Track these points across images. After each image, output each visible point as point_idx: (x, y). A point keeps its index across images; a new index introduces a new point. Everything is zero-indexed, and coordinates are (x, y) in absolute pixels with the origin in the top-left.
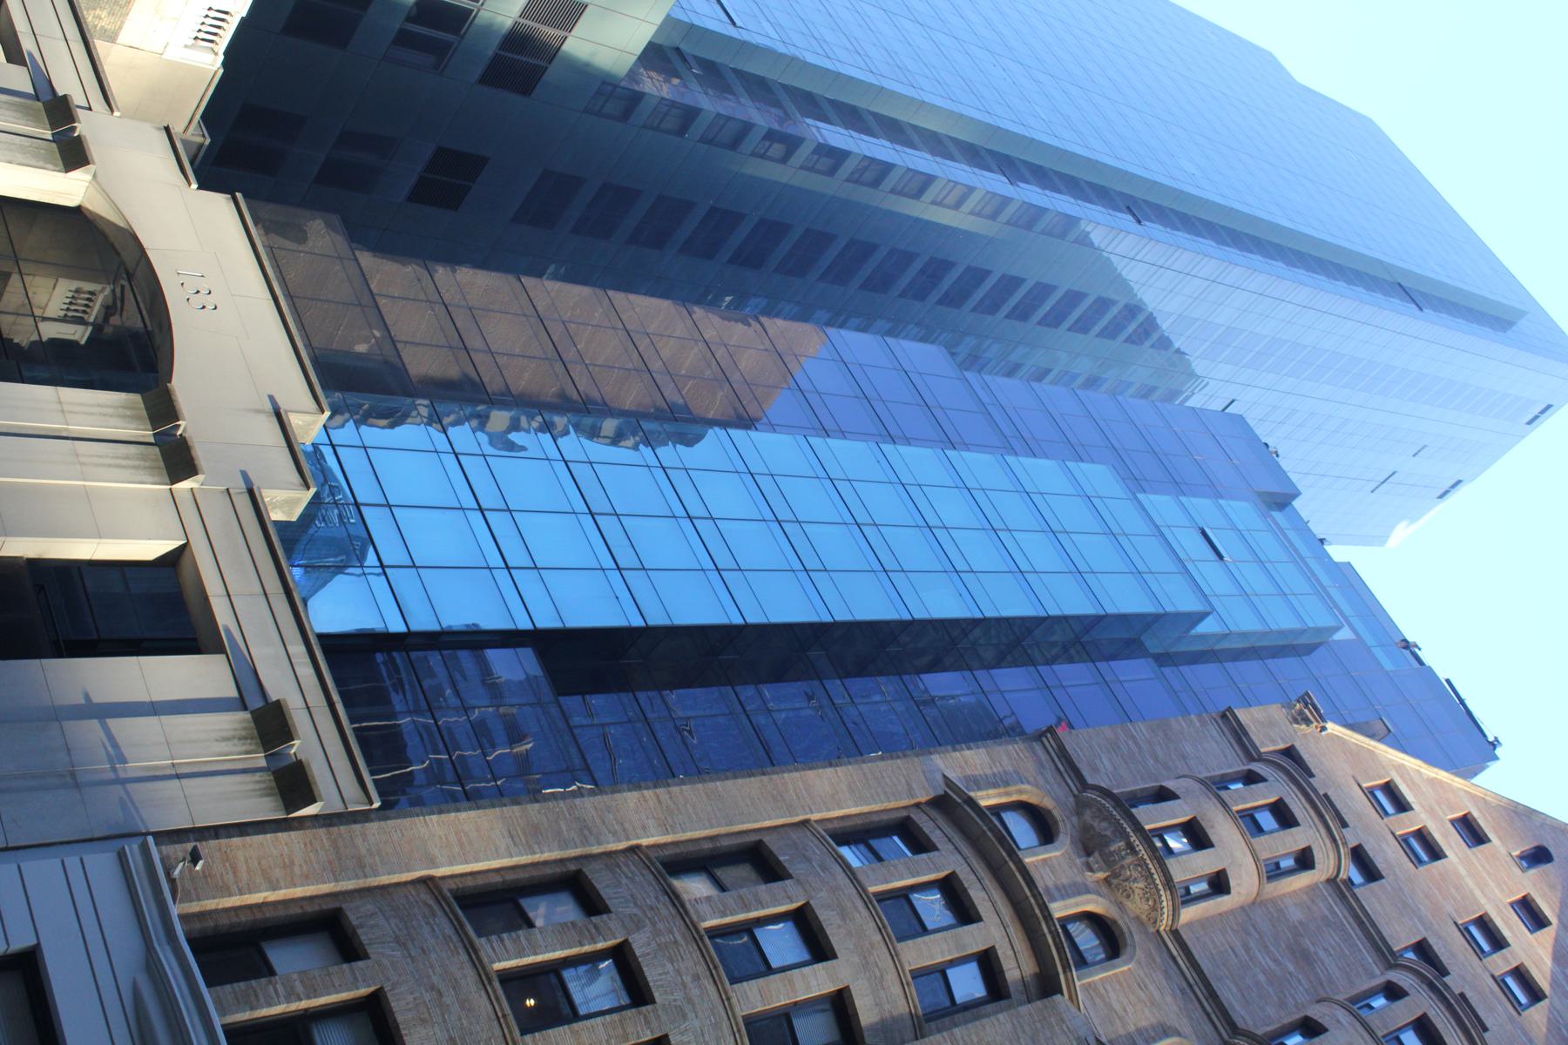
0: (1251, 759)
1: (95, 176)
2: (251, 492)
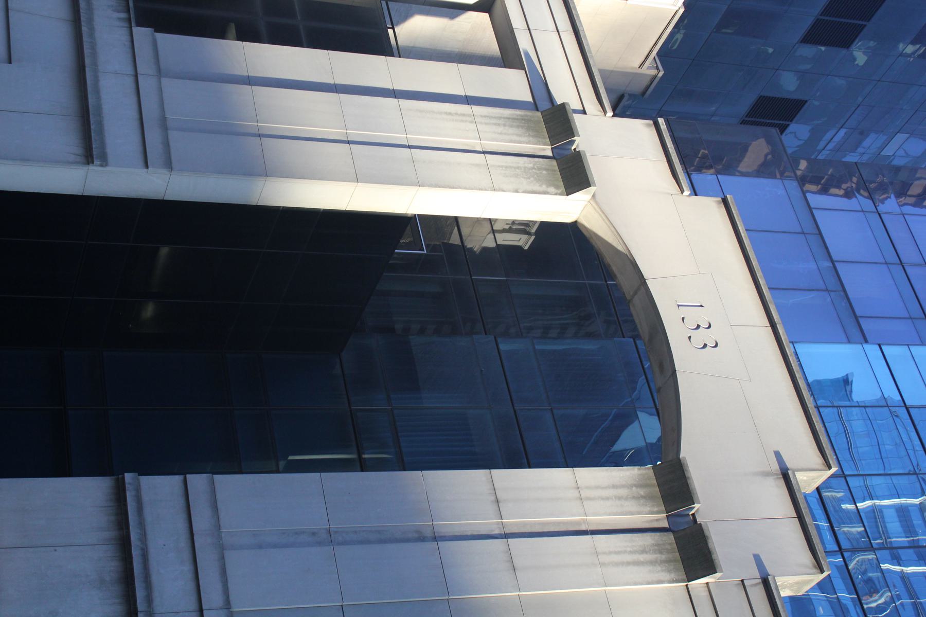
1: (594, 196)
2: (766, 583)
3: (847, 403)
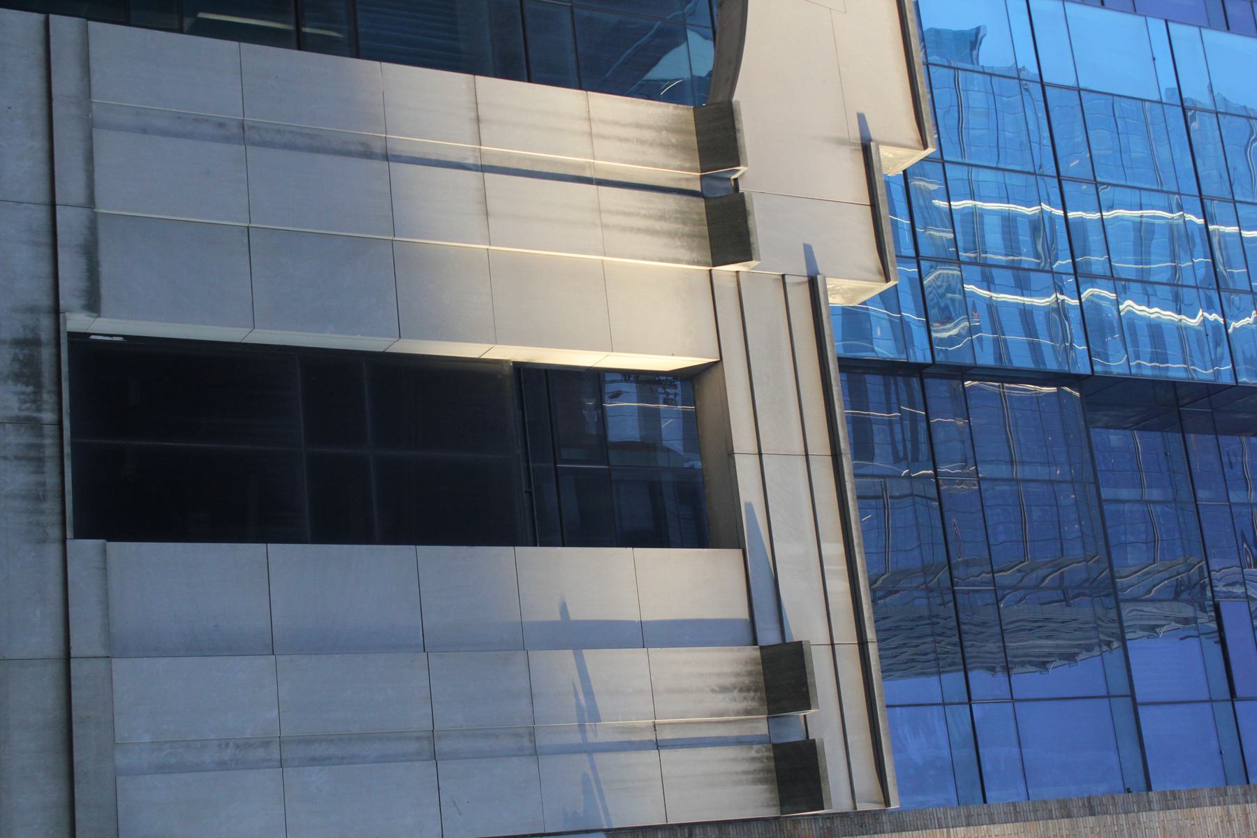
2: (813, 283)
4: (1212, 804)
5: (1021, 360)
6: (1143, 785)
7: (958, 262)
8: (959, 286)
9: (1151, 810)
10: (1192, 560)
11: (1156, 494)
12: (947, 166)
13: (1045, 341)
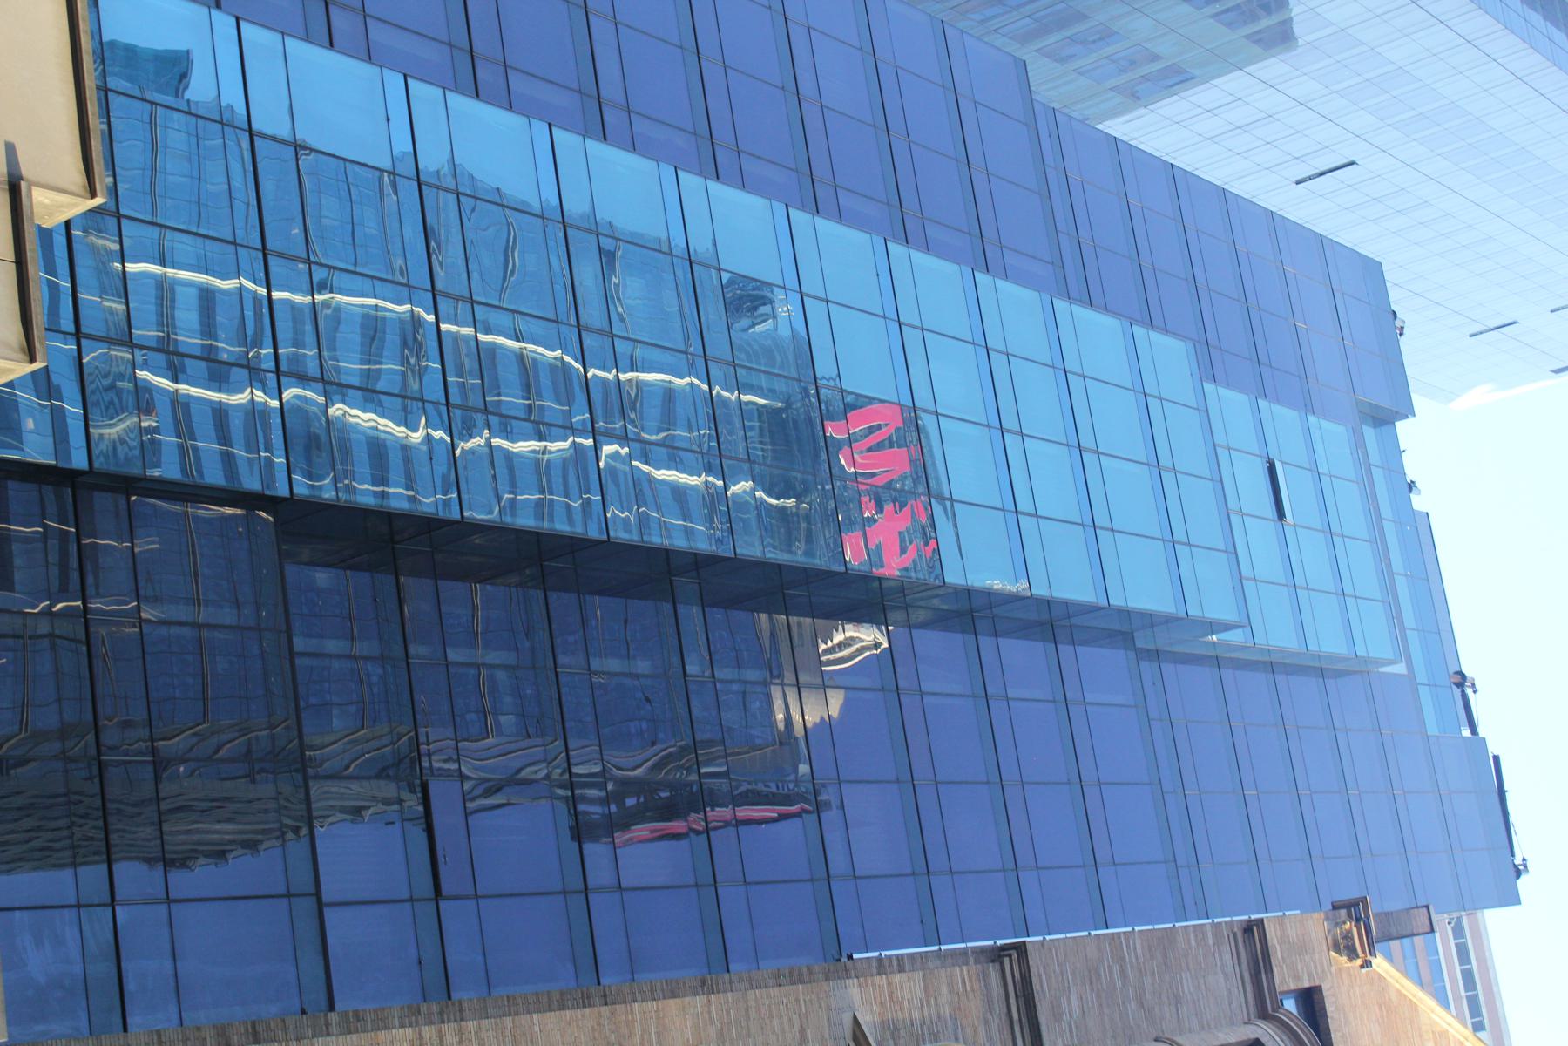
0: (1264, 1015)
3: (169, 100)
4: (402, 1026)
5: (214, 476)
6: (324, 1004)
7: (129, 342)
8: (129, 370)
9: (328, 1034)
10: (403, 729)
11: (363, 647)
12: (124, 222)
13: (239, 452)
